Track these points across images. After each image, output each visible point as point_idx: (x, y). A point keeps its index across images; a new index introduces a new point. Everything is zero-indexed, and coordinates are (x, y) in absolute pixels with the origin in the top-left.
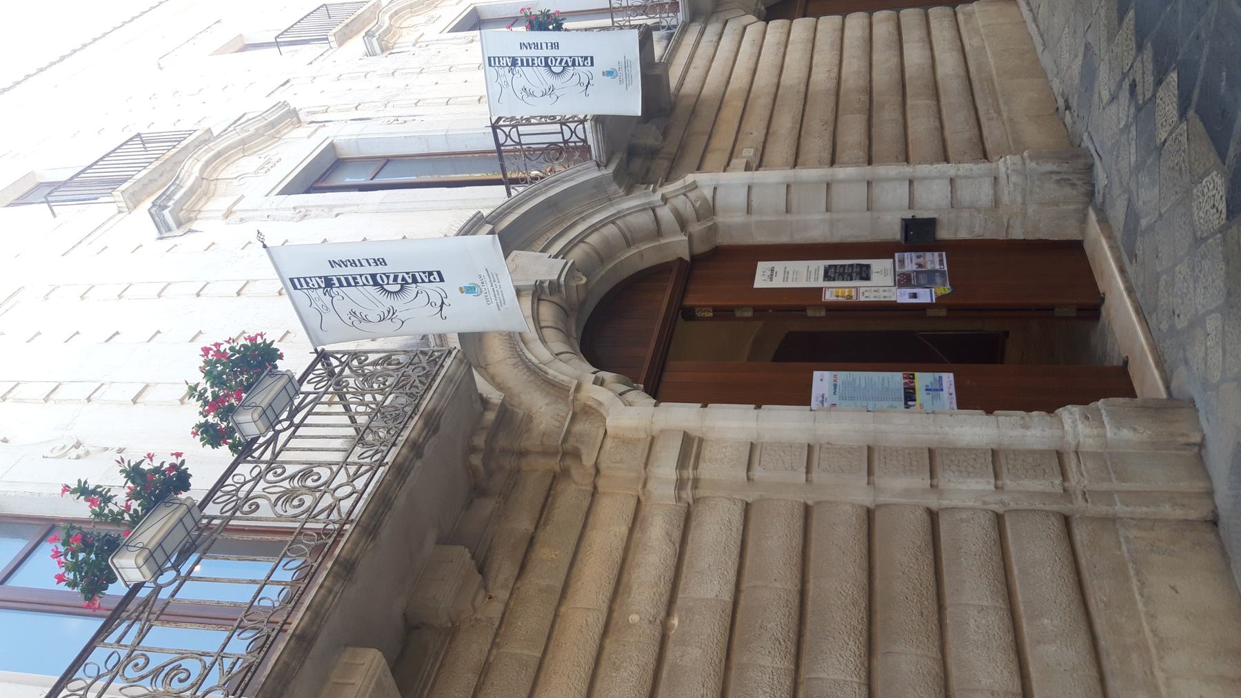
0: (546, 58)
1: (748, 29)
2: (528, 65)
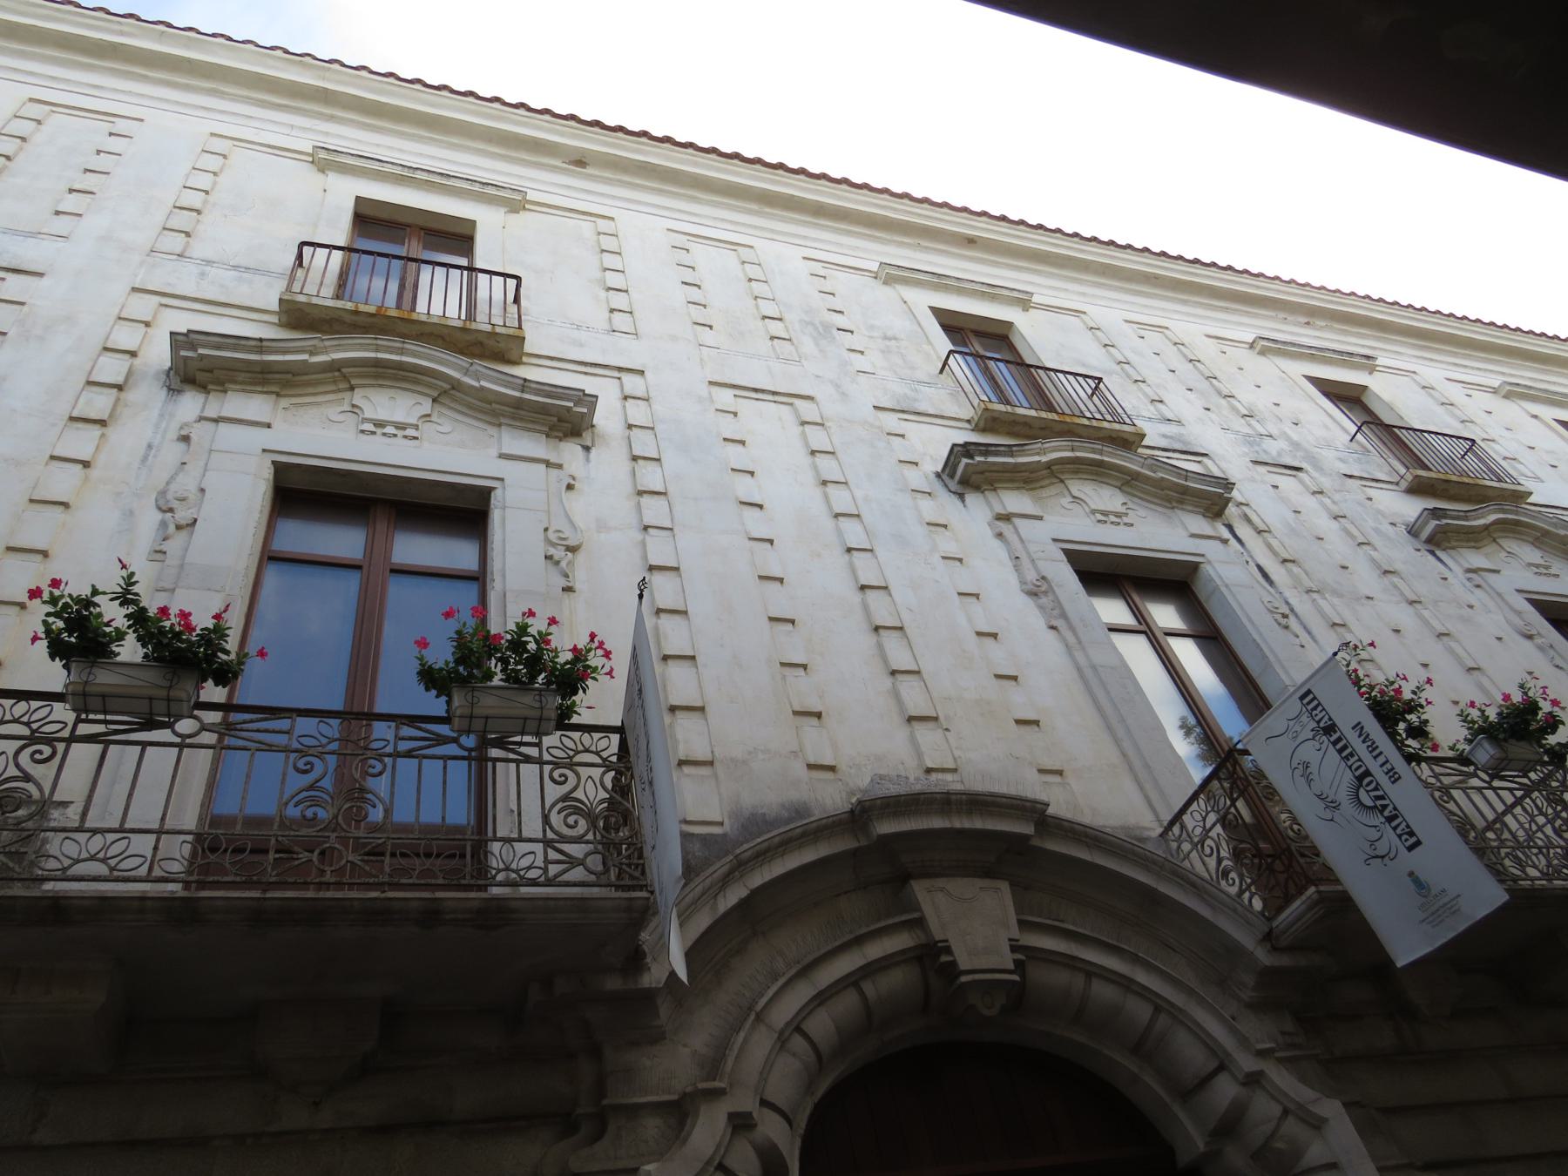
0: (1367, 773)
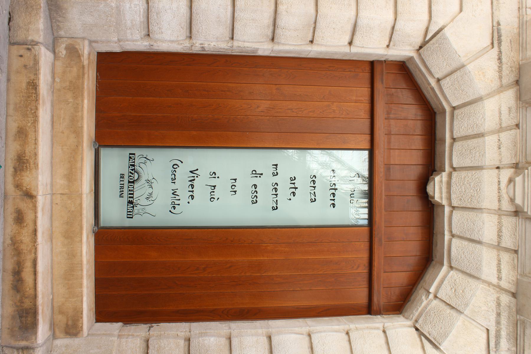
0: (129, 182)
2: (133, 194)
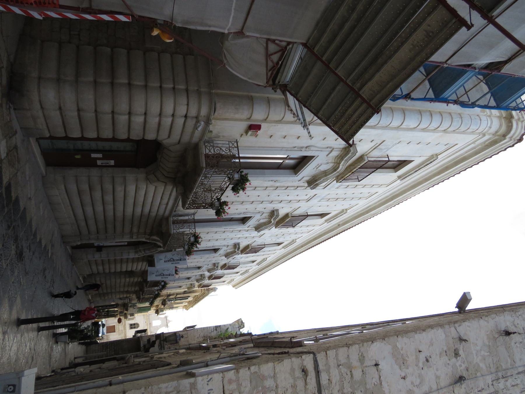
1: (167, 137)
